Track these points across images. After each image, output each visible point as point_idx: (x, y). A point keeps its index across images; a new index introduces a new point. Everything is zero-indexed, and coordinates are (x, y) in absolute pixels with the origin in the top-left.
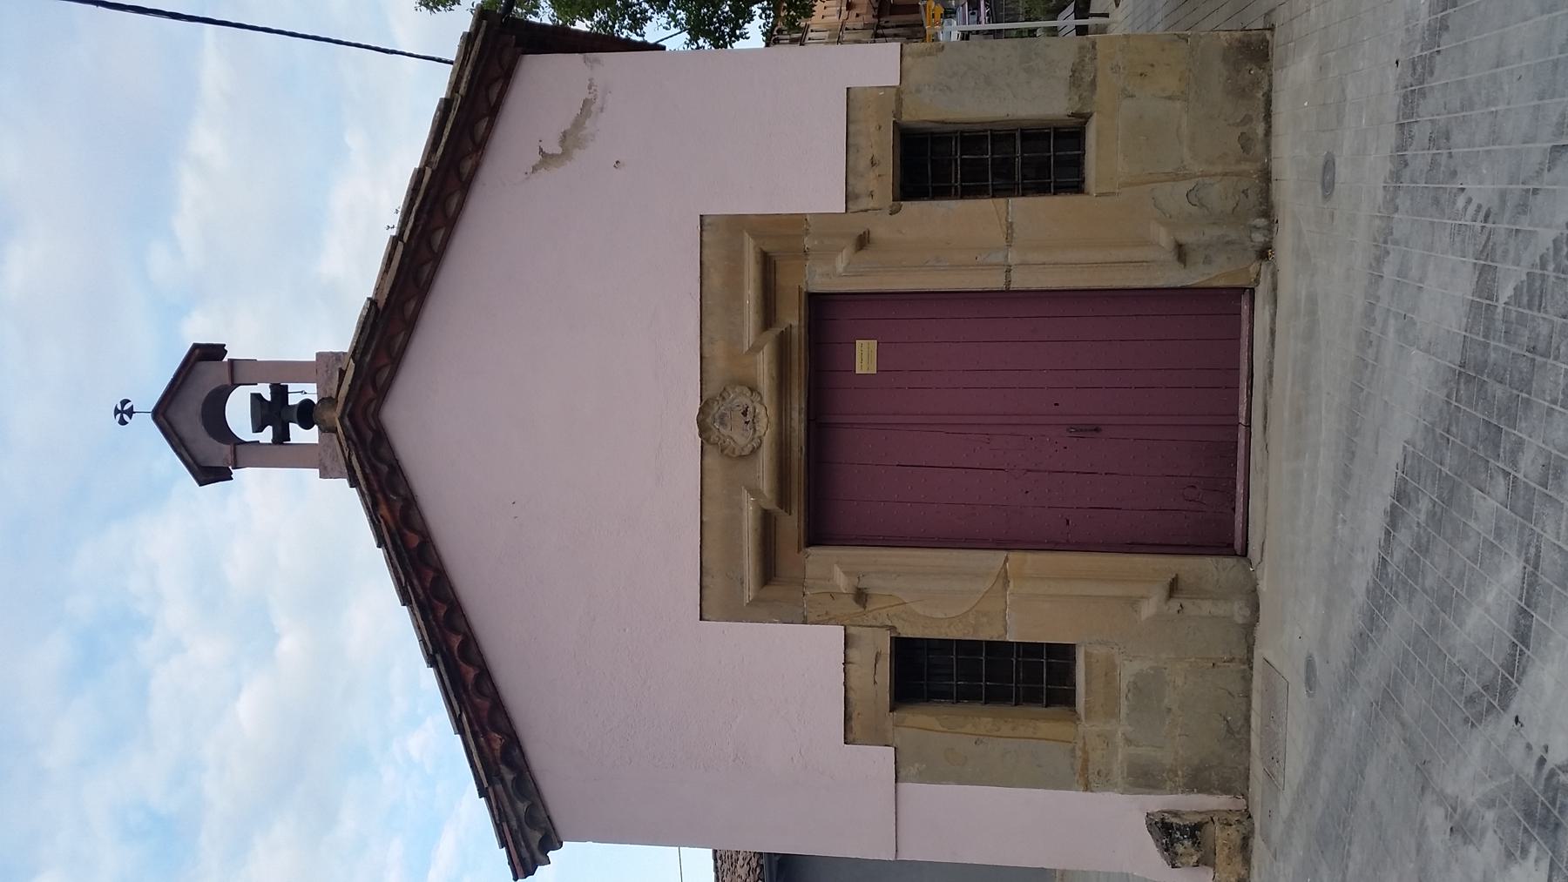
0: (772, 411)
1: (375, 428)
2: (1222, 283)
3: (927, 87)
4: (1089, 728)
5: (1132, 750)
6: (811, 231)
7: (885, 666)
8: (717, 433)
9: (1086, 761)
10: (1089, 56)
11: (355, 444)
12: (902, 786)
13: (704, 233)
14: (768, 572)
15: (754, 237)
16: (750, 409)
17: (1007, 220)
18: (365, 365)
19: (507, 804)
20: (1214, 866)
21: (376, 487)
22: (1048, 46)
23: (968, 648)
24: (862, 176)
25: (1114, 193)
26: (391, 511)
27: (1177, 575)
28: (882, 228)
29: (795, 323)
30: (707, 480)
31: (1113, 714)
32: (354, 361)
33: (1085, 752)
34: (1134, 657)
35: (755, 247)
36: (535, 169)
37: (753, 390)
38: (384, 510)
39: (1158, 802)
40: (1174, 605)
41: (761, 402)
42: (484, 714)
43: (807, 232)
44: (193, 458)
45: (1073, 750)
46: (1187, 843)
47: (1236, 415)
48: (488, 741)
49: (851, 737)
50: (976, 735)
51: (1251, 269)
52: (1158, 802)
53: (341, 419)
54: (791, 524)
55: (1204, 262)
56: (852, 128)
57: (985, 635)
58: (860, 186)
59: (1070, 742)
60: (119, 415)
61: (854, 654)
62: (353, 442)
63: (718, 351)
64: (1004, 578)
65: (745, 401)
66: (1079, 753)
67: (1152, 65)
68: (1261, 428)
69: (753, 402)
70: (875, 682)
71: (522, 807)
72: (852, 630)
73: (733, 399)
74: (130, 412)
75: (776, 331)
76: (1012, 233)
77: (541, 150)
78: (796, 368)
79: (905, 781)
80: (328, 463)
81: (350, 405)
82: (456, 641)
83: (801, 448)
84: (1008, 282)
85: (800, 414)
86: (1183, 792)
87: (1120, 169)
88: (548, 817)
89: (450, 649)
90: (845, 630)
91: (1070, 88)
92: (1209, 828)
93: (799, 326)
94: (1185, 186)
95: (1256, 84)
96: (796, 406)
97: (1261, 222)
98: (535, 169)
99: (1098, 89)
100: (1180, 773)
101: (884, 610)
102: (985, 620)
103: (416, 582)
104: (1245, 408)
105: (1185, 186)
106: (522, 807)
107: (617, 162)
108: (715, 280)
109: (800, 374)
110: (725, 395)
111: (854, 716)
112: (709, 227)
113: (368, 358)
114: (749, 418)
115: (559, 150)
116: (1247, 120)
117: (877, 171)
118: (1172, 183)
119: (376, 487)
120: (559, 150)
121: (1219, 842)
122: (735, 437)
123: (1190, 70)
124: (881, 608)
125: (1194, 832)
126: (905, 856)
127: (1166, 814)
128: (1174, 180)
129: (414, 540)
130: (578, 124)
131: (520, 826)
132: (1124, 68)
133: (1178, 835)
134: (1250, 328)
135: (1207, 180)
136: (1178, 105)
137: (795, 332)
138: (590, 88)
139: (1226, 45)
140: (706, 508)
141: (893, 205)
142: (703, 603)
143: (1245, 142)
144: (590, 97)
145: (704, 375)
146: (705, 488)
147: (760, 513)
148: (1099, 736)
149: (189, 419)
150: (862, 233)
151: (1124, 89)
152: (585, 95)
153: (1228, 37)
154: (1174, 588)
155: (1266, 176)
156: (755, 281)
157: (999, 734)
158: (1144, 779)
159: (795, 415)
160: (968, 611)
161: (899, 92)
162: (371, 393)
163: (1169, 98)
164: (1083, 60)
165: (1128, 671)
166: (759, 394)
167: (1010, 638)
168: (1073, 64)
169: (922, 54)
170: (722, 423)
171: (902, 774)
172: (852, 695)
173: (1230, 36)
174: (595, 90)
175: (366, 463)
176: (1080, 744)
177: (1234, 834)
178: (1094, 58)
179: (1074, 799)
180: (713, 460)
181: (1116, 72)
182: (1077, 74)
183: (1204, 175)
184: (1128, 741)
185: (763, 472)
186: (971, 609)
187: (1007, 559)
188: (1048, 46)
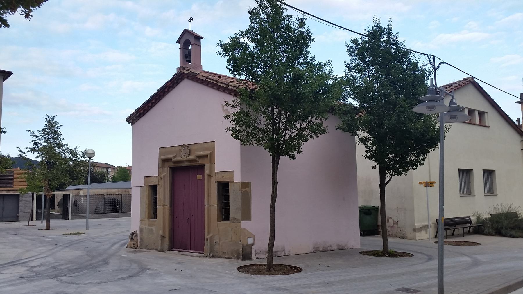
0: (185, 159)
11: (178, 75)
19: (134, 115)
21: (172, 81)
25: (217, 226)
26: (169, 85)
29: (199, 163)
30: (178, 147)
37: (189, 155)
38: (169, 83)
39: (138, 232)
42: (145, 109)
45: (144, 218)
48: (141, 110)
52: (138, 232)
54: (172, 165)
68: (182, 254)
71: (134, 118)
78: (193, 163)
82: (153, 101)
88: (135, 123)
89: (152, 100)
92: (133, 241)
94: (218, 240)
95: (233, 256)
97: (211, 255)
103: (160, 92)
105: (218, 240)
106: (134, 118)
111: (148, 178)
117: (222, 178)
119: (172, 81)
129: (166, 90)
131: (132, 118)
136: (230, 240)
137: (198, 163)
143: (224, 253)
147: (207, 155)
155: (219, 257)
158: (141, 230)
159: (186, 164)
162: (186, 76)
163: (231, 238)
169: (239, 187)
170: (184, 149)
171: (142, 187)
172: (150, 178)
178: (238, 223)
179: (139, 219)
184: (145, 228)
185: (178, 159)
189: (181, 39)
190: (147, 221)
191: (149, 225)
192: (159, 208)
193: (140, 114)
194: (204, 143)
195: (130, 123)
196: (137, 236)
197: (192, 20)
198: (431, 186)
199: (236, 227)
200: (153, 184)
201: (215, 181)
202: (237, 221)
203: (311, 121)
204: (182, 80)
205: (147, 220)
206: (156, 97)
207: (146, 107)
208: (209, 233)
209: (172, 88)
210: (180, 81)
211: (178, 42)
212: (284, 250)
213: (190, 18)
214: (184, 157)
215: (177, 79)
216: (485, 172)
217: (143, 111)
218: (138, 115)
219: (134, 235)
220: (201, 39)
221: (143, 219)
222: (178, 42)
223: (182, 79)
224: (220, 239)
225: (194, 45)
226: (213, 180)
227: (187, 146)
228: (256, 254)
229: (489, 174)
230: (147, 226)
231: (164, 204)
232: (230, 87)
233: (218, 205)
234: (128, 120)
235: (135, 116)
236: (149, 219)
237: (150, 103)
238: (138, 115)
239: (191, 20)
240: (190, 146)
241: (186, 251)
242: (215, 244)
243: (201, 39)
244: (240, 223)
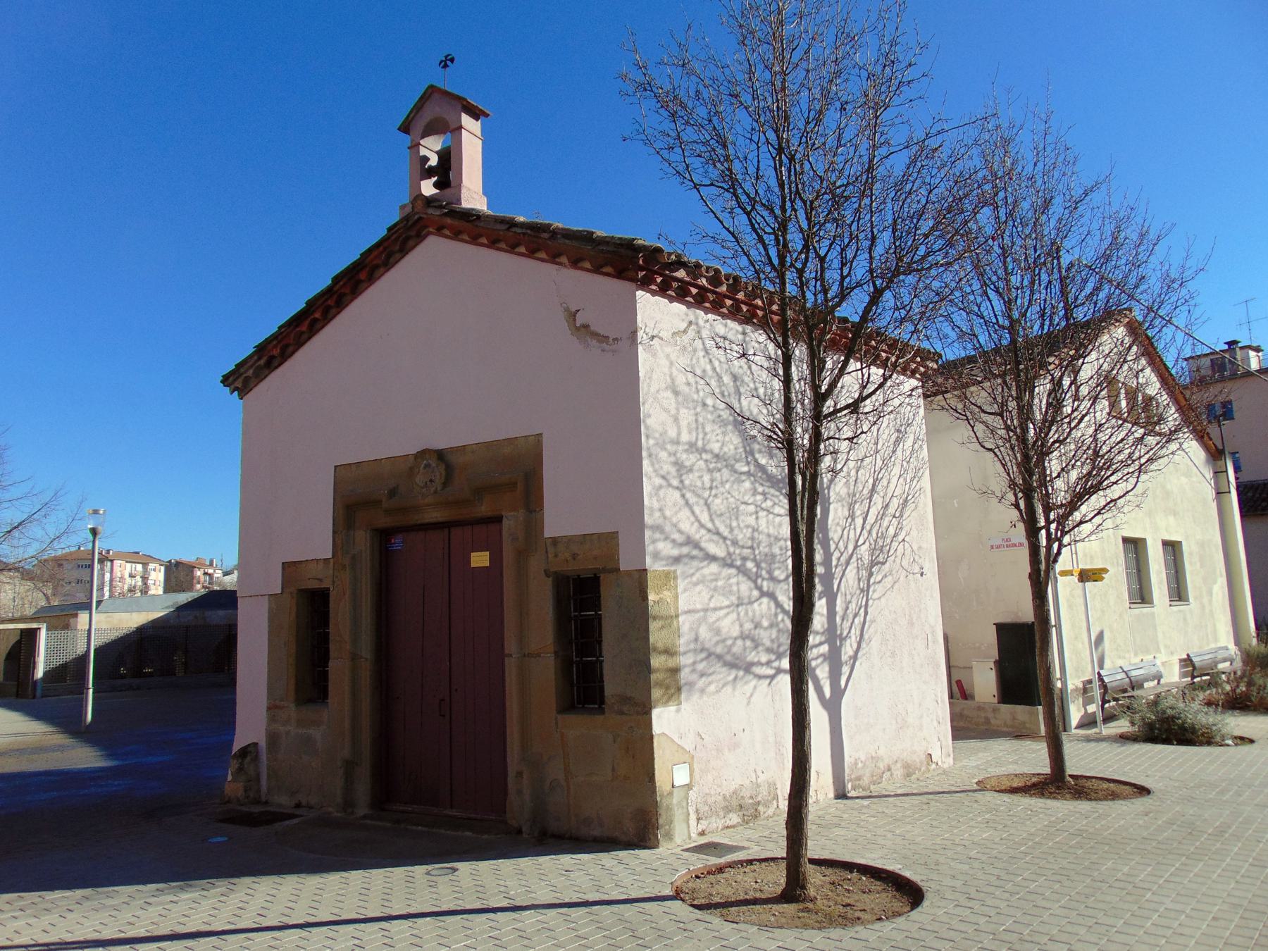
10: (640, 709)
44: (413, 118)
48: (275, 346)
57: (332, 647)
62: (406, 224)
82: (317, 315)
88: (251, 390)
107: (446, 66)
115: (578, 325)
120: (578, 325)
126: (239, 600)
129: (362, 276)
130: (595, 335)
158: (273, 739)
167: (331, 663)
178: (638, 713)
184: (288, 733)
189: (415, 116)
190: (292, 710)
192: (338, 668)
193: (272, 358)
195: (236, 392)
196: (256, 758)
198: (1096, 581)
200: (314, 585)
201: (545, 571)
203: (898, 358)
204: (421, 241)
205: (292, 706)
206: (326, 300)
207: (292, 335)
209: (382, 270)
210: (411, 243)
212: (774, 799)
213: (446, 57)
215: (401, 239)
216: (1166, 543)
217: (281, 349)
218: (262, 362)
219: (248, 759)
221: (278, 703)
223: (420, 238)
226: (536, 564)
228: (698, 819)
229: (1172, 548)
233: (556, 653)
234: (226, 380)
235: (251, 366)
237: (307, 323)
238: (262, 362)
239: (449, 63)
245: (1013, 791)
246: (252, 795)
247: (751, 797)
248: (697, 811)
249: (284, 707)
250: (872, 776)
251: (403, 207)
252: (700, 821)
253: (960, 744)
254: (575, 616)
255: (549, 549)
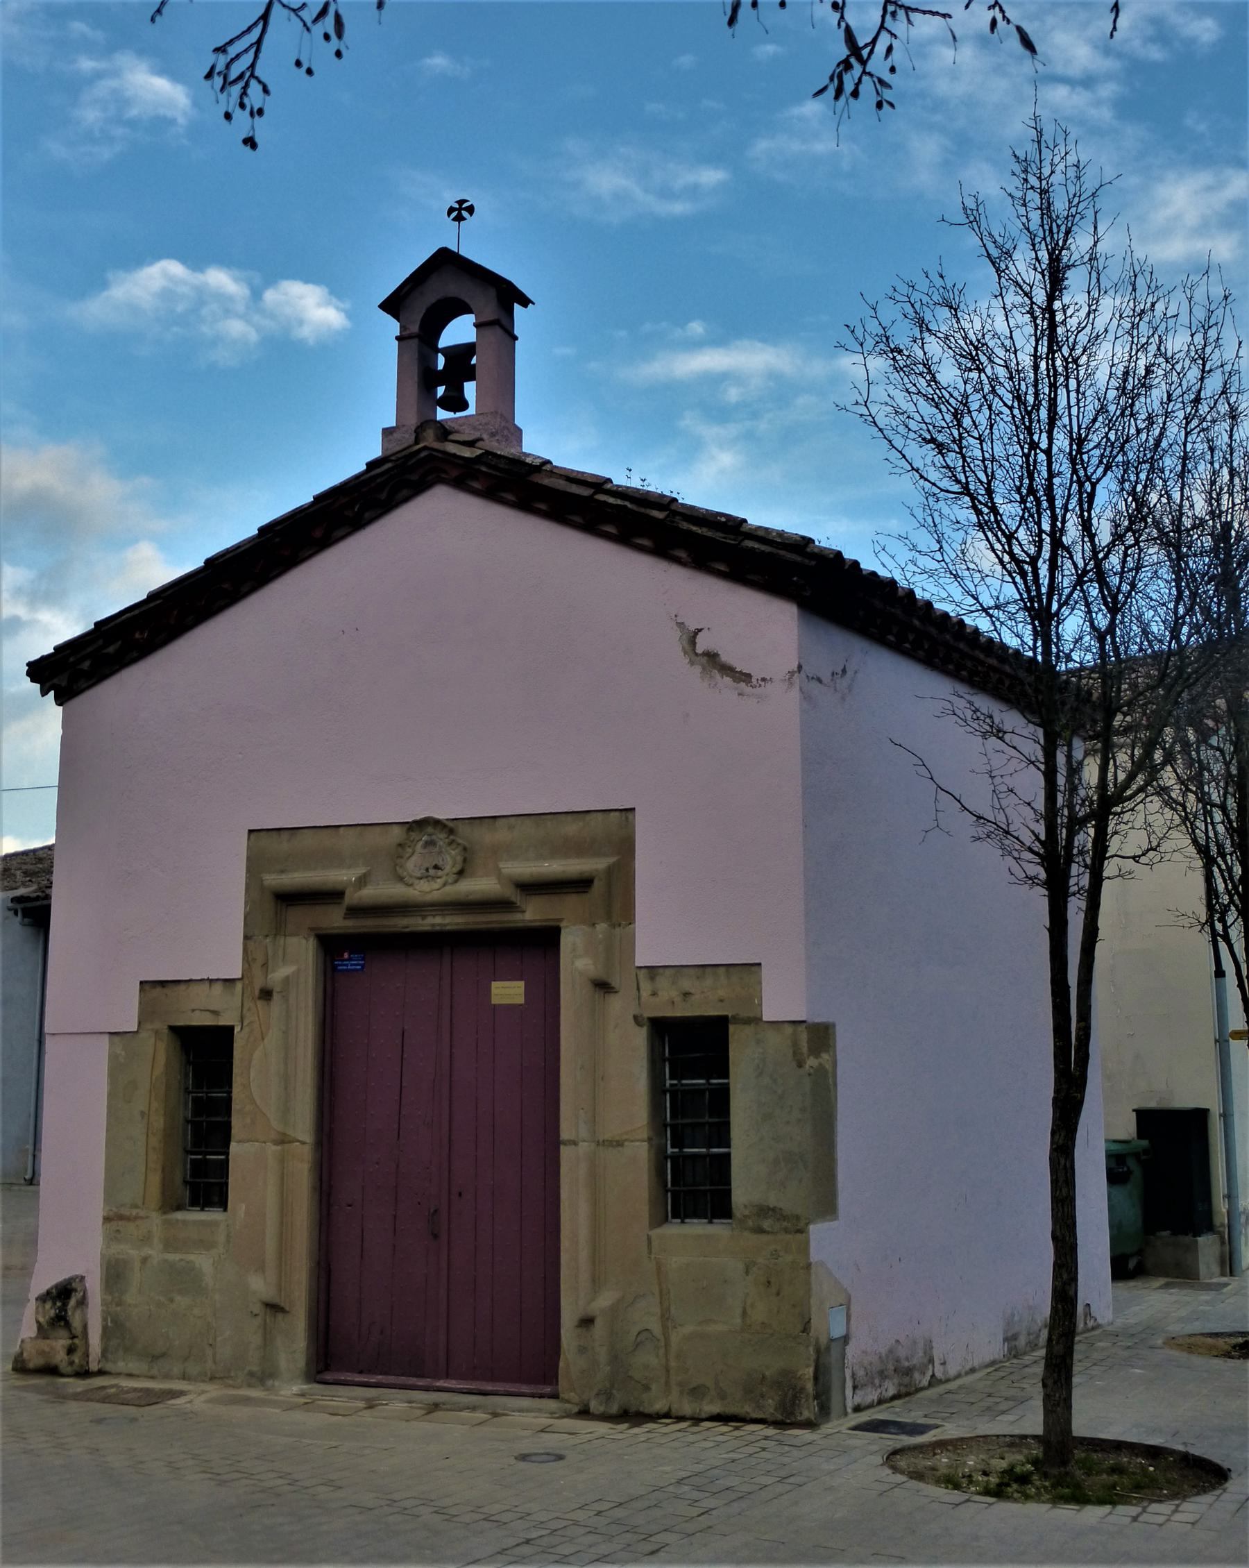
0: (436, 896)
1: (544, 468)
2: (561, 1364)
3: (761, 1050)
4: (156, 1220)
5: (137, 1265)
6: (618, 929)
7: (207, 1020)
8: (417, 838)
9: (128, 1219)
12: (106, 1038)
13: (617, 814)
14: (289, 899)
15: (609, 871)
16: (440, 873)
17: (626, 1140)
18: (477, 467)
20: (37, 1338)
22: (800, 1181)
23: (225, 1106)
24: (673, 983)
25: (650, 1252)
27: (288, 1312)
28: (619, 1007)
30: (378, 829)
31: (169, 1245)
32: (482, 454)
33: (137, 1218)
34: (216, 1268)
35: (597, 870)
36: (681, 625)
37: (461, 873)
39: (94, 1287)
40: (257, 1308)
41: (445, 885)
43: (613, 926)
45: (136, 1207)
46: (52, 1313)
47: (448, 1376)
49: (147, 987)
50: (149, 1111)
51: (572, 1394)
52: (94, 1287)
53: (425, 448)
54: (335, 920)
55: (580, 1346)
56: (722, 970)
58: (663, 982)
59: (143, 1203)
60: (457, 206)
61: (218, 988)
63: (502, 835)
64: (283, 1140)
65: (448, 868)
66: (134, 1212)
67: (778, 1294)
69: (447, 875)
70: (193, 1011)
72: (239, 986)
73: (449, 854)
74: (459, 218)
75: (515, 896)
76: (613, 1146)
77: (700, 630)
79: (111, 1044)
80: (396, 435)
81: (440, 455)
83: (407, 927)
84: (565, 1143)
85: (439, 925)
86: (103, 1311)
87: (674, 1259)
90: (238, 979)
91: (757, 1206)
93: (523, 921)
94: (656, 1328)
96: (448, 920)
98: (681, 625)
99: (756, 1236)
100: (119, 1308)
101: (257, 1019)
102: (248, 1121)
104: (453, 1386)
107: (459, 218)
108: (571, 828)
109: (478, 923)
110: (454, 846)
111: (165, 991)
112: (623, 818)
113: (484, 469)
114: (432, 872)
115: (699, 650)
116: (722, 1396)
117: (678, 999)
118: (659, 1314)
120: (699, 650)
121: (54, 1343)
122: (414, 858)
123: (772, 1335)
124: (258, 1017)
125: (61, 1320)
127: (81, 1294)
128: (662, 1316)
130: (727, 670)
132: (776, 1264)
133: (59, 1304)
134: (384, 1384)
135: (662, 1351)
137: (518, 916)
138: (764, 680)
139: (800, 1373)
140: (353, 829)
141: (644, 1019)
142: (264, 832)
144: (754, 680)
145: (477, 821)
146: (370, 828)
148: (149, 1232)
149: (445, 286)
150: (613, 985)
151: (755, 1263)
152: (756, 675)
153: (807, 1377)
154: (273, 1308)
156: (564, 872)
157: (150, 1134)
158: (115, 1274)
160: (256, 1104)
161: (756, 1020)
162: (455, 473)
164: (784, 1220)
165: (203, 1262)
166: (456, 881)
167: (234, 1147)
168: (781, 1209)
169: (795, 1044)
171: (116, 1039)
172: (182, 987)
173: (809, 1379)
174: (760, 685)
175: (386, 477)
176: (142, 1213)
177: (60, 1358)
178: (786, 1231)
179: (97, 1210)
180: (397, 834)
181: (772, 1254)
182: (770, 1213)
183: (667, 1345)
184: (145, 1260)
185: (383, 890)
186: (258, 1107)
187: (303, 1143)
188: (800, 1181)
191: (170, 1244)
194: (563, 817)
195: (52, 693)
197: (471, 214)
199: (775, 1254)
202: (785, 1224)
208: (597, 1283)
211: (392, 305)
214: (424, 886)
220: (517, 307)
222: (392, 305)
223: (419, 488)
224: (665, 1318)
225: (497, 327)
227: (446, 827)
228: (855, 1388)
230: (155, 1253)
231: (284, 1134)
232: (750, 544)
236: (165, 1213)
239: (465, 214)
240: (463, 829)
241: (421, 1382)
242: (637, 1345)
243: (517, 307)
244: (800, 1231)
245: (1191, 1348)
246: (77, 1361)
247: (907, 1359)
248: (853, 1375)
249: (137, 1218)
250: (1029, 1334)
251: (387, 432)
252: (857, 1391)
253: (1115, 1285)
254: (671, 1085)
255: (642, 985)
